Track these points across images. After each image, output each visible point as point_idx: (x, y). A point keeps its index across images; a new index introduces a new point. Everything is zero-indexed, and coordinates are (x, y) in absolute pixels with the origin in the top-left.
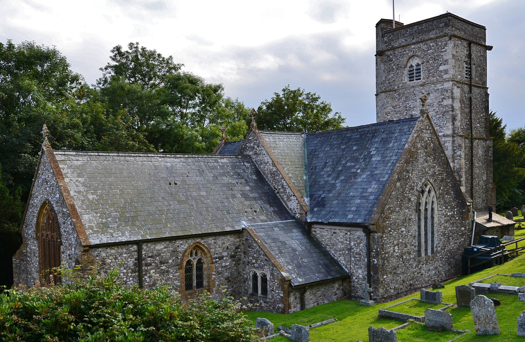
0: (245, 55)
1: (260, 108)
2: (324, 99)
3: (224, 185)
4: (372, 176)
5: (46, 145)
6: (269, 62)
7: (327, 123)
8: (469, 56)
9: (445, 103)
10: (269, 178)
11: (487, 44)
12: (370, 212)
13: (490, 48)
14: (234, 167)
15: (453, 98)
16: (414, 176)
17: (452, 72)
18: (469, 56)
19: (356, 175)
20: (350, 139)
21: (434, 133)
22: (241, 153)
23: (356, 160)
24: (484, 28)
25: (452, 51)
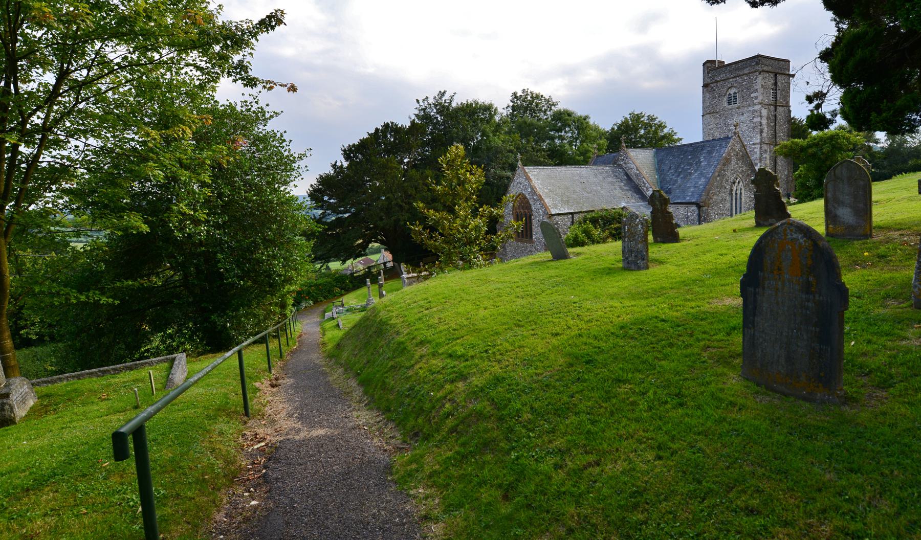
0: (569, 72)
1: (613, 129)
2: (660, 118)
3: (609, 183)
4: (701, 174)
5: (520, 164)
6: (592, 76)
7: (664, 137)
8: (776, 84)
9: (755, 120)
10: (634, 178)
11: (791, 73)
12: (701, 195)
13: (793, 76)
14: (613, 172)
15: (761, 117)
16: (728, 173)
17: (760, 98)
18: (776, 84)
19: (691, 174)
20: (686, 152)
21: (743, 145)
22: (615, 163)
23: (691, 165)
24: (788, 61)
25: (761, 82)
